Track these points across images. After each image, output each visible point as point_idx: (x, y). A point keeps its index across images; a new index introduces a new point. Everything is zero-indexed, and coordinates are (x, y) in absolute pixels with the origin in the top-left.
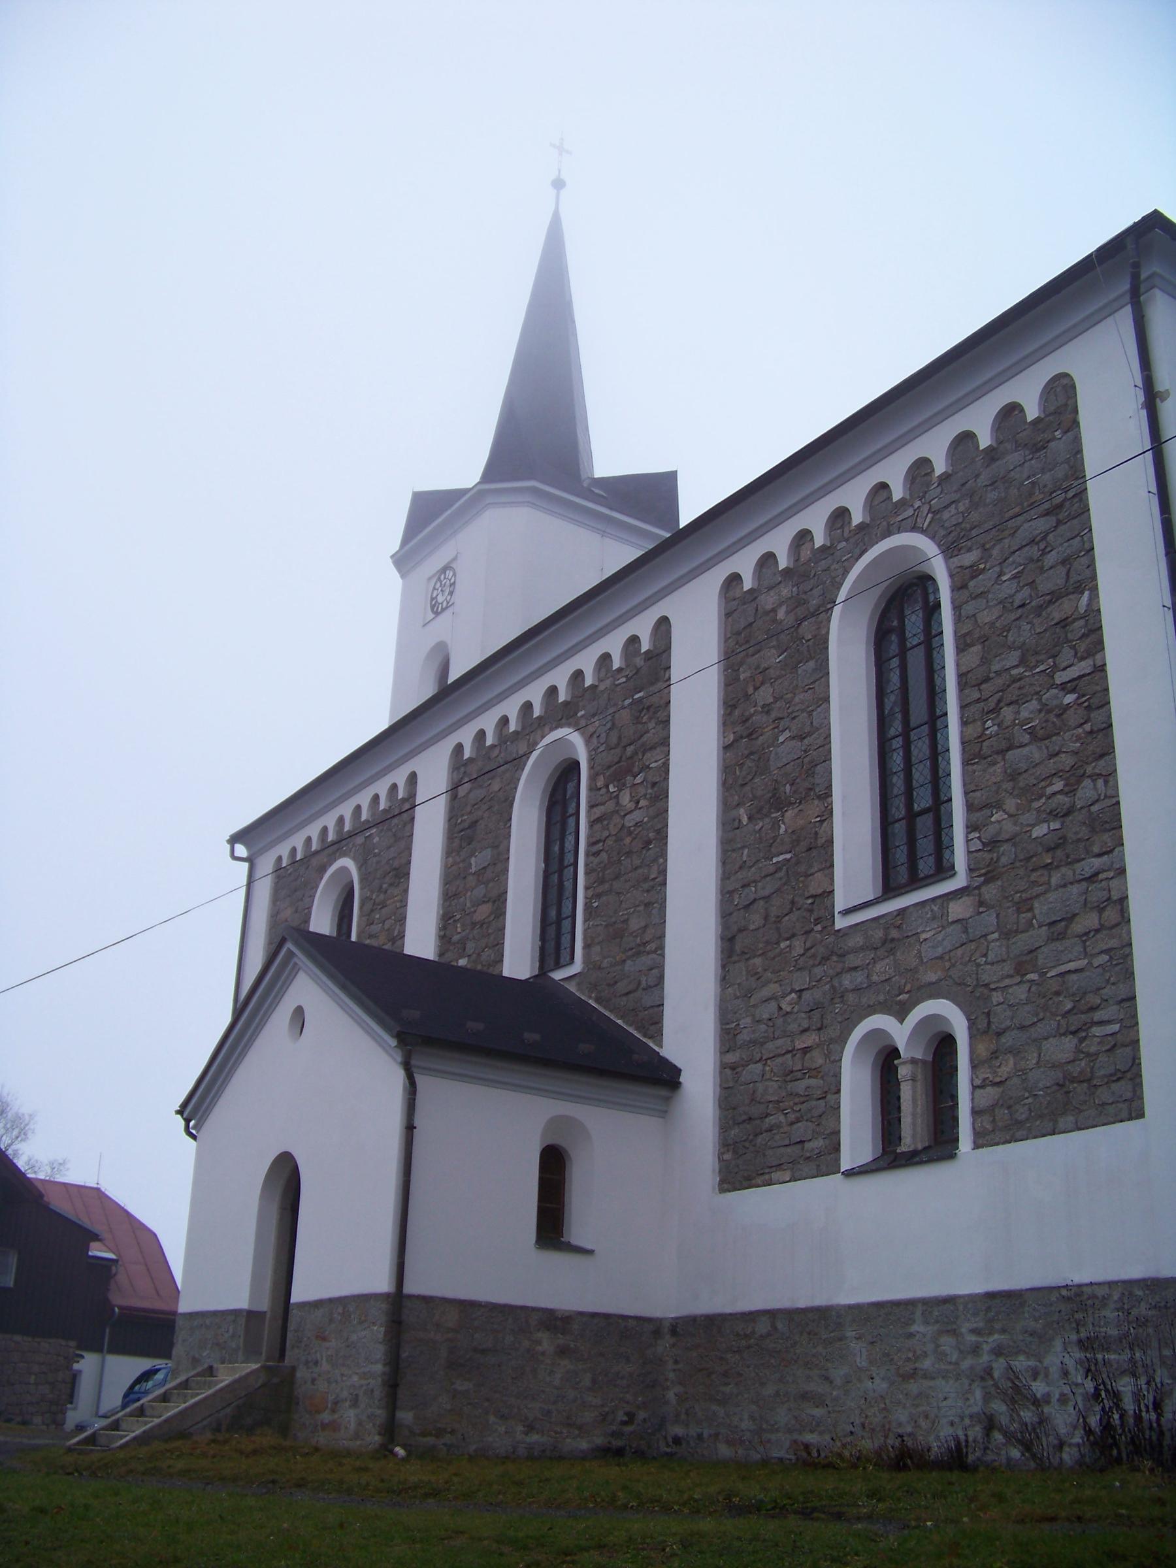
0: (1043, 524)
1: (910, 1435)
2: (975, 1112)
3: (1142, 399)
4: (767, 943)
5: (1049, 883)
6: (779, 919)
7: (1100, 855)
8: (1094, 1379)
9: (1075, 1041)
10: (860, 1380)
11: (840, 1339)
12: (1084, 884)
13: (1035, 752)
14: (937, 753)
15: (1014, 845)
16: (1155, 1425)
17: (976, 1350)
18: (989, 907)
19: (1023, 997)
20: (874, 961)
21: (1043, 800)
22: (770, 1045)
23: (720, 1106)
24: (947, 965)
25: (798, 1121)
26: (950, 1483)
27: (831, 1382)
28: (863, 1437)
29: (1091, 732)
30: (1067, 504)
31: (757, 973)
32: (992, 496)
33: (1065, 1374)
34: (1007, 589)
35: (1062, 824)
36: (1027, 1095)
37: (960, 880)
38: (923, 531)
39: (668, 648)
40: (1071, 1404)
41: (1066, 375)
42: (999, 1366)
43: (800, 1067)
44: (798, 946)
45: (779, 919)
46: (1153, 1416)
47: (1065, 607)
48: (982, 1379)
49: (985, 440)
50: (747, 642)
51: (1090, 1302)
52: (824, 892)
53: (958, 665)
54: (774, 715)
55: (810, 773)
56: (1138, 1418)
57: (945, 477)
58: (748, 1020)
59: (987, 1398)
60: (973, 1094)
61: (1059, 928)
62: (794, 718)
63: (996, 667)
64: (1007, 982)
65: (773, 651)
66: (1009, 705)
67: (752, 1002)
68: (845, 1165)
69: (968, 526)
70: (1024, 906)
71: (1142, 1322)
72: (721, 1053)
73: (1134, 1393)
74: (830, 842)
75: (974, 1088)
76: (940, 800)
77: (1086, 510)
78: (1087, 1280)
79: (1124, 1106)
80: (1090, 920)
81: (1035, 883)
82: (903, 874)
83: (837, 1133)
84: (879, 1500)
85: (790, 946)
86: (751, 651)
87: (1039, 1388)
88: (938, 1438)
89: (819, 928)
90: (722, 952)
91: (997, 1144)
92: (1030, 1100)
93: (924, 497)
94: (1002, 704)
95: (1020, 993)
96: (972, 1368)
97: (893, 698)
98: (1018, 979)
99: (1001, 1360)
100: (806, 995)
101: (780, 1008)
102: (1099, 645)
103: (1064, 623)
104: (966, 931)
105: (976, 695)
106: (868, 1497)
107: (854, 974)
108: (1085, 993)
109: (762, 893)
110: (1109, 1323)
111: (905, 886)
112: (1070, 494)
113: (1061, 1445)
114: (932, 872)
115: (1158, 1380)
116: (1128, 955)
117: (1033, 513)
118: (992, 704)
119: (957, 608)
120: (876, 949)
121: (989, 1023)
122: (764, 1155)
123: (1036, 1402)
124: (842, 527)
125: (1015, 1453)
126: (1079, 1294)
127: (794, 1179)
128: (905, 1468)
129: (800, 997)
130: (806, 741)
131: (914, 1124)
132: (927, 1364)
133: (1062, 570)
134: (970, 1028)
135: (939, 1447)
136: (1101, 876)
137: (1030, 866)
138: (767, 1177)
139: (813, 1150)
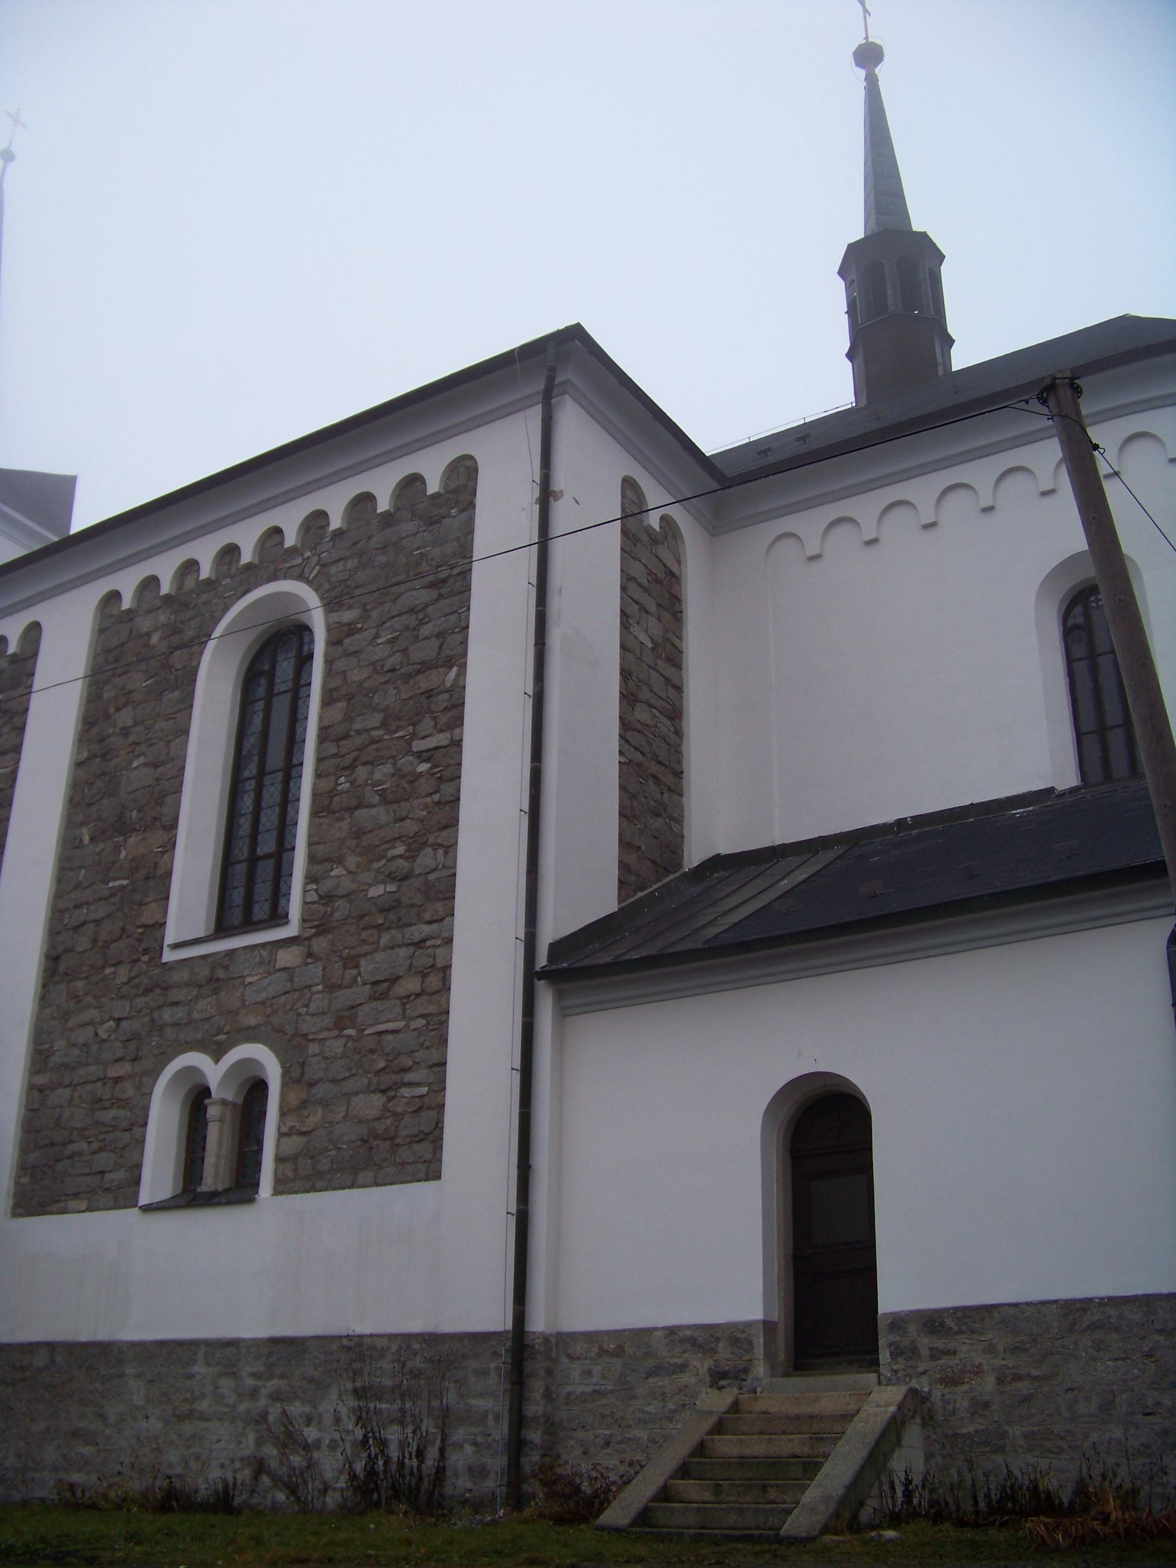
0: (424, 596)
1: (179, 1476)
2: (279, 1159)
3: (537, 494)
4: (93, 967)
5: (378, 943)
6: (107, 944)
7: (430, 922)
8: (364, 1426)
9: (384, 1099)
10: (135, 1419)
11: (119, 1376)
12: (412, 949)
13: (382, 814)
14: (288, 801)
15: (350, 902)
16: (415, 1471)
17: (254, 1394)
18: (317, 959)
19: (339, 1051)
20: (197, 998)
21: (383, 862)
22: (82, 1071)
23: (23, 1127)
24: (269, 1010)
25: (101, 1150)
26: (213, 1526)
27: (105, 1420)
28: (131, 1478)
29: (438, 803)
30: (451, 580)
31: (77, 997)
32: (381, 559)
33: (338, 1420)
34: (380, 652)
35: (399, 887)
36: (331, 1147)
37: (291, 930)
38: (309, 582)
39: (35, 655)
40: (340, 1449)
41: (471, 458)
42: (275, 1411)
43: (109, 1096)
44: (123, 974)
45: (107, 944)
46: (415, 1463)
47: (424, 682)
48: (257, 1422)
49: (383, 504)
50: (116, 661)
51: (369, 1353)
52: (157, 923)
53: (321, 718)
54: (132, 738)
55: (160, 803)
56: (401, 1464)
57: (339, 533)
58: (63, 1043)
59: (259, 1442)
60: (278, 1141)
61: (382, 988)
62: (150, 745)
63: (357, 725)
64: (325, 1034)
65: (141, 675)
66: (364, 764)
67: (70, 1024)
68: (144, 1199)
69: (352, 584)
70: (352, 962)
71: (416, 1374)
72: (30, 1074)
73: (400, 1441)
74: (169, 874)
75: (281, 1135)
76: (284, 848)
77: (468, 589)
78: (368, 1331)
79: (423, 1167)
80: (411, 985)
81: (364, 942)
82: (237, 916)
83: (139, 1166)
84: (137, 1544)
85: (114, 973)
86: (118, 671)
87: (311, 1434)
88: (206, 1481)
89: (146, 958)
90: (45, 971)
91: (297, 1192)
92: (333, 1153)
93: (315, 548)
94: (357, 763)
95: (337, 1046)
96: (248, 1411)
97: (252, 740)
98: (336, 1033)
99: (278, 1405)
100: (125, 1025)
101: (96, 1035)
102: (458, 721)
103: (429, 694)
104: (291, 980)
105: (334, 750)
106: (126, 1540)
107: (175, 1009)
108: (399, 1054)
109: (93, 916)
110: (384, 1374)
111: (237, 927)
112: (456, 571)
113: (325, 1490)
114: (265, 917)
115: (424, 1429)
116: (443, 1023)
117: (417, 584)
118: (348, 761)
119: (329, 662)
120: (200, 986)
121: (303, 1073)
122: (62, 1181)
123: (306, 1447)
124: (230, 563)
125: (281, 1497)
126: (360, 1345)
127: (90, 1209)
128: (171, 1509)
129: (118, 1026)
130: (160, 770)
131: (217, 1165)
132: (204, 1405)
133: (435, 643)
134: (283, 1075)
135: (206, 1489)
136: (428, 943)
137: (362, 924)
138: (62, 1205)
139: (112, 1181)
